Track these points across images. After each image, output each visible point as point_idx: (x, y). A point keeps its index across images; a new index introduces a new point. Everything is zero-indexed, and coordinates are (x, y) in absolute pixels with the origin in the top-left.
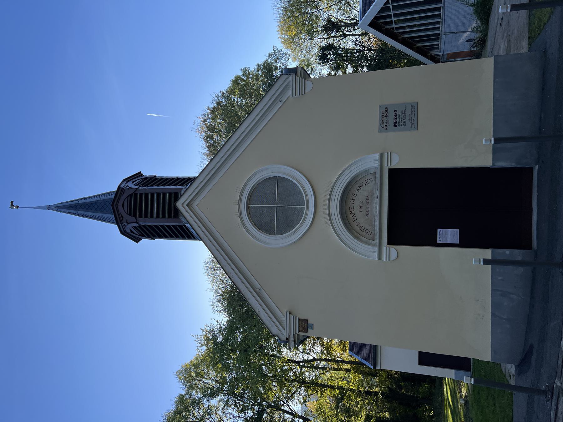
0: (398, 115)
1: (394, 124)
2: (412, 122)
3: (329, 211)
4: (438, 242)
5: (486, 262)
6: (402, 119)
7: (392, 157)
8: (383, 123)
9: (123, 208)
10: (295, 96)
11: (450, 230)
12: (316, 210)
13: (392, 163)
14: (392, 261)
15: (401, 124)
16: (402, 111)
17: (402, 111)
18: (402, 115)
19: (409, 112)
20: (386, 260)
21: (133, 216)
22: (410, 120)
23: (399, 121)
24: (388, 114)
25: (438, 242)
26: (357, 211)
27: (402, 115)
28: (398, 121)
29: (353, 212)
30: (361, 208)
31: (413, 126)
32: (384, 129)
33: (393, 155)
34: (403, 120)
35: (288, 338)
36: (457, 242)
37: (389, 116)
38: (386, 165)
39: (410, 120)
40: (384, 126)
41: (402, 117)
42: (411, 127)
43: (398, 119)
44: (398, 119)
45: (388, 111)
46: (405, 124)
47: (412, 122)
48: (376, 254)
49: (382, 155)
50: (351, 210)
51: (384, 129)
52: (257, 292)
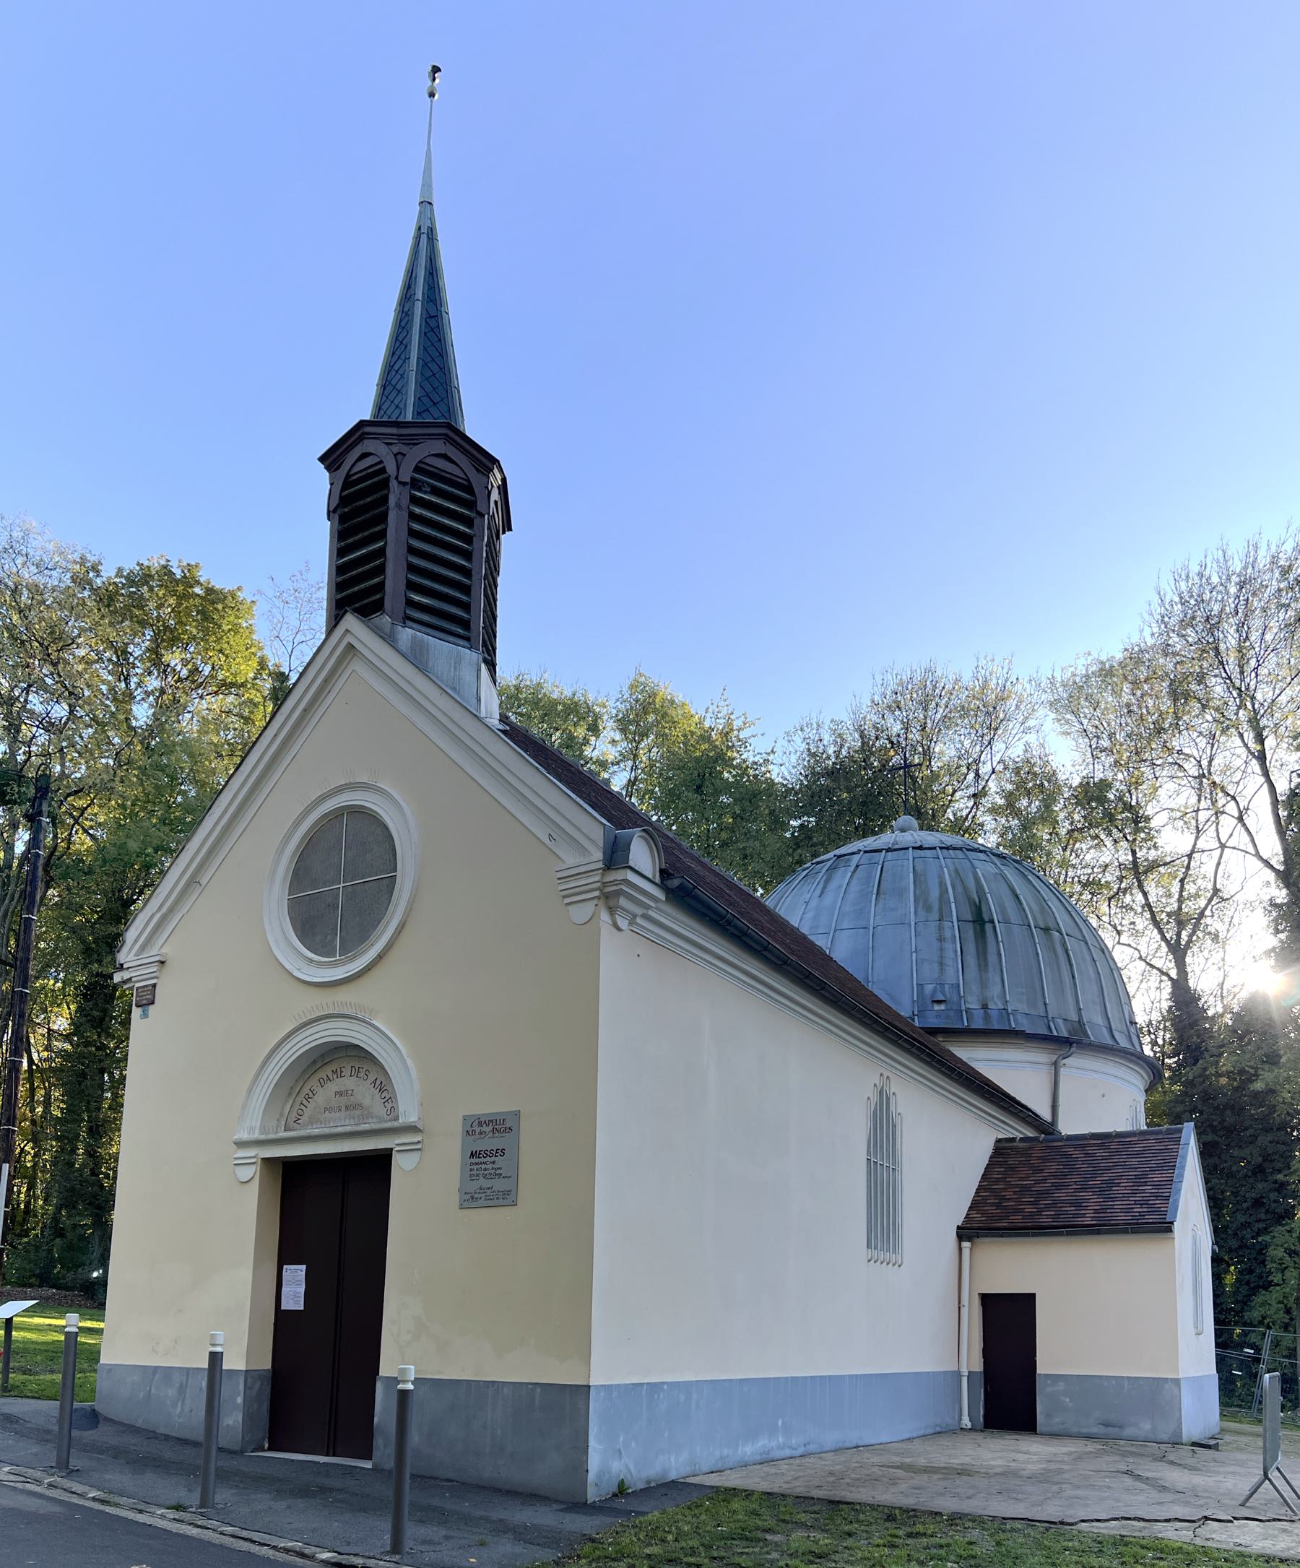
0: (493, 1159)
1: (476, 1152)
2: (476, 1196)
3: (321, 1019)
4: (285, 1267)
5: (215, 1358)
6: (485, 1169)
7: (412, 1153)
8: (480, 1124)
9: (436, 455)
10: (559, 879)
11: (302, 1289)
12: (341, 984)
13: (402, 1154)
14: (234, 1172)
15: (475, 1167)
16: (500, 1168)
17: (500, 1168)
18: (493, 1169)
19: (499, 1184)
20: (235, 1158)
21: (341, 497)
22: (481, 1189)
23: (481, 1163)
24: (497, 1135)
25: (285, 1267)
26: (333, 1087)
27: (493, 1169)
28: (483, 1160)
29: (335, 1076)
30: (341, 1094)
31: (468, 1197)
32: (470, 1129)
33: (417, 1155)
34: (481, 1173)
35: (125, 966)
36: (285, 1306)
37: (493, 1137)
38: (397, 1142)
39: (481, 1189)
40: (476, 1126)
41: (488, 1169)
42: (466, 1193)
43: (485, 1160)
44: (485, 1160)
45: (504, 1134)
46: (473, 1177)
47: (476, 1196)
48: (245, 1136)
49: (412, 1129)
50: (339, 1070)
51: (470, 1129)
52: (193, 881)
